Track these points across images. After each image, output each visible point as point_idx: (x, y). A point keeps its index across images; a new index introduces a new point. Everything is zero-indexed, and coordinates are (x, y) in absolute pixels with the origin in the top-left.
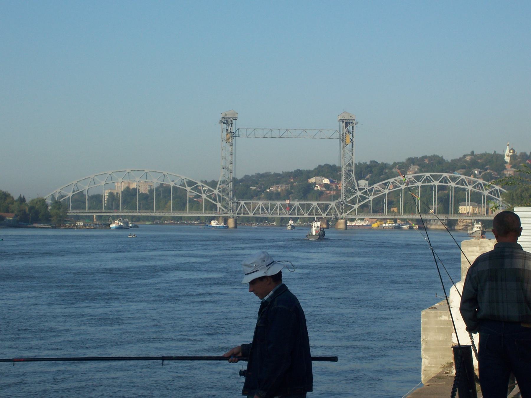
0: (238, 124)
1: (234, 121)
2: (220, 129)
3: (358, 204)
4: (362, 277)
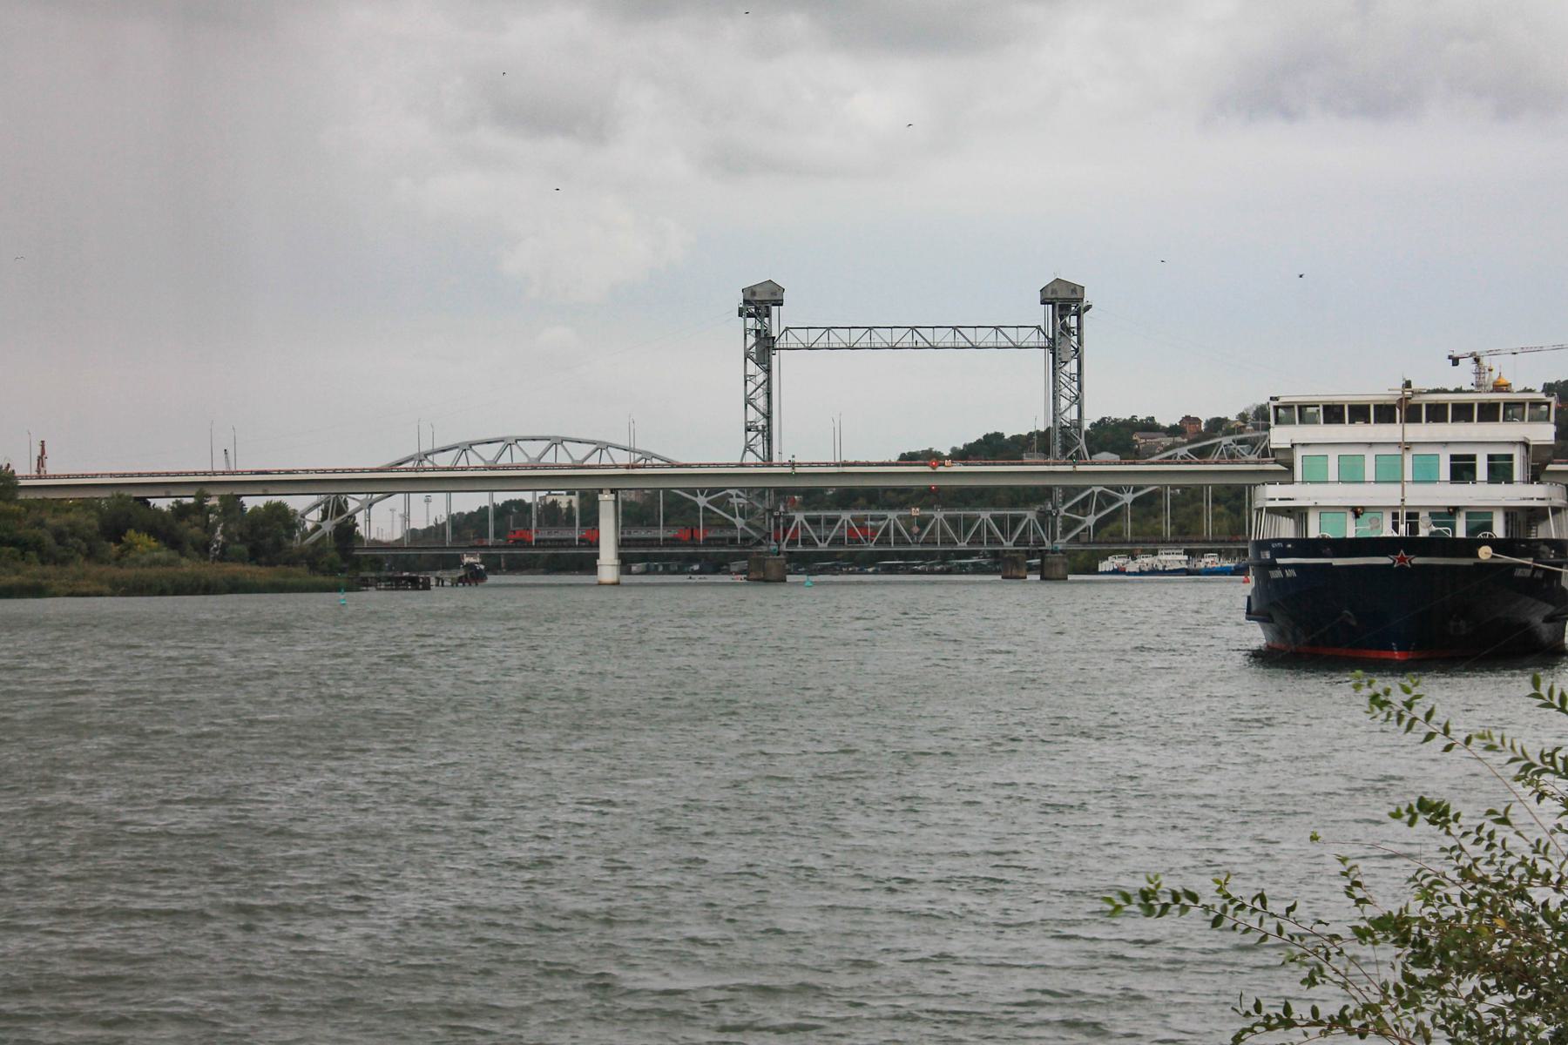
0: (779, 319)
1: (774, 309)
2: (735, 334)
3: (1095, 514)
4: (1030, 668)
